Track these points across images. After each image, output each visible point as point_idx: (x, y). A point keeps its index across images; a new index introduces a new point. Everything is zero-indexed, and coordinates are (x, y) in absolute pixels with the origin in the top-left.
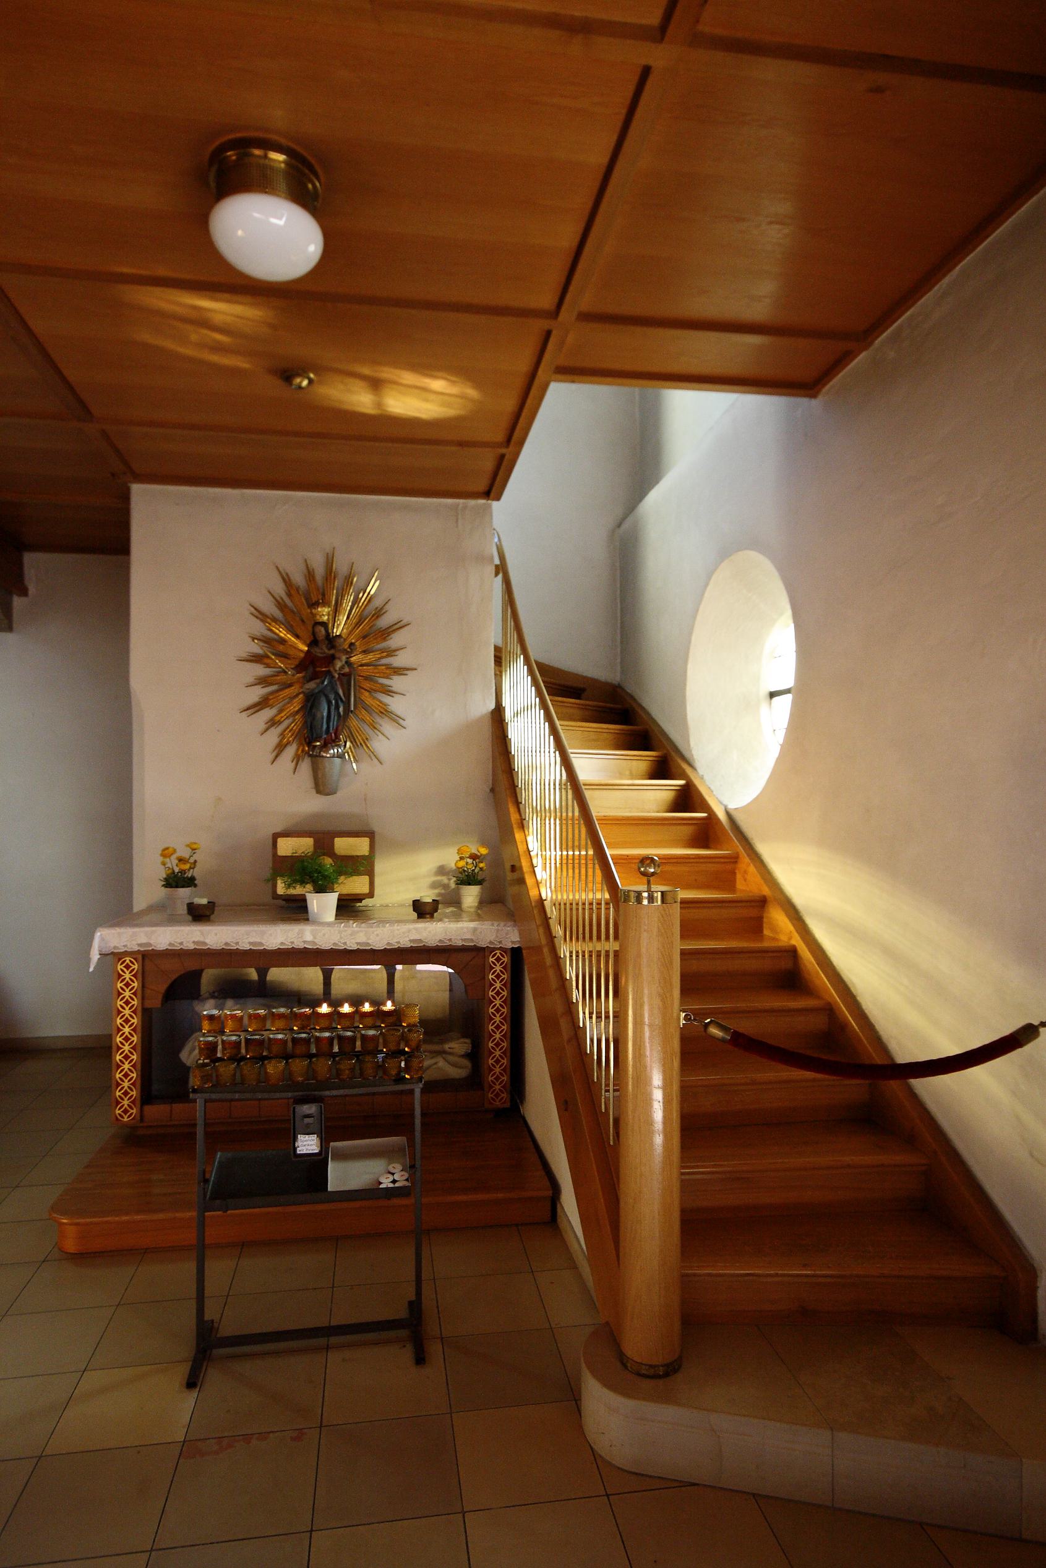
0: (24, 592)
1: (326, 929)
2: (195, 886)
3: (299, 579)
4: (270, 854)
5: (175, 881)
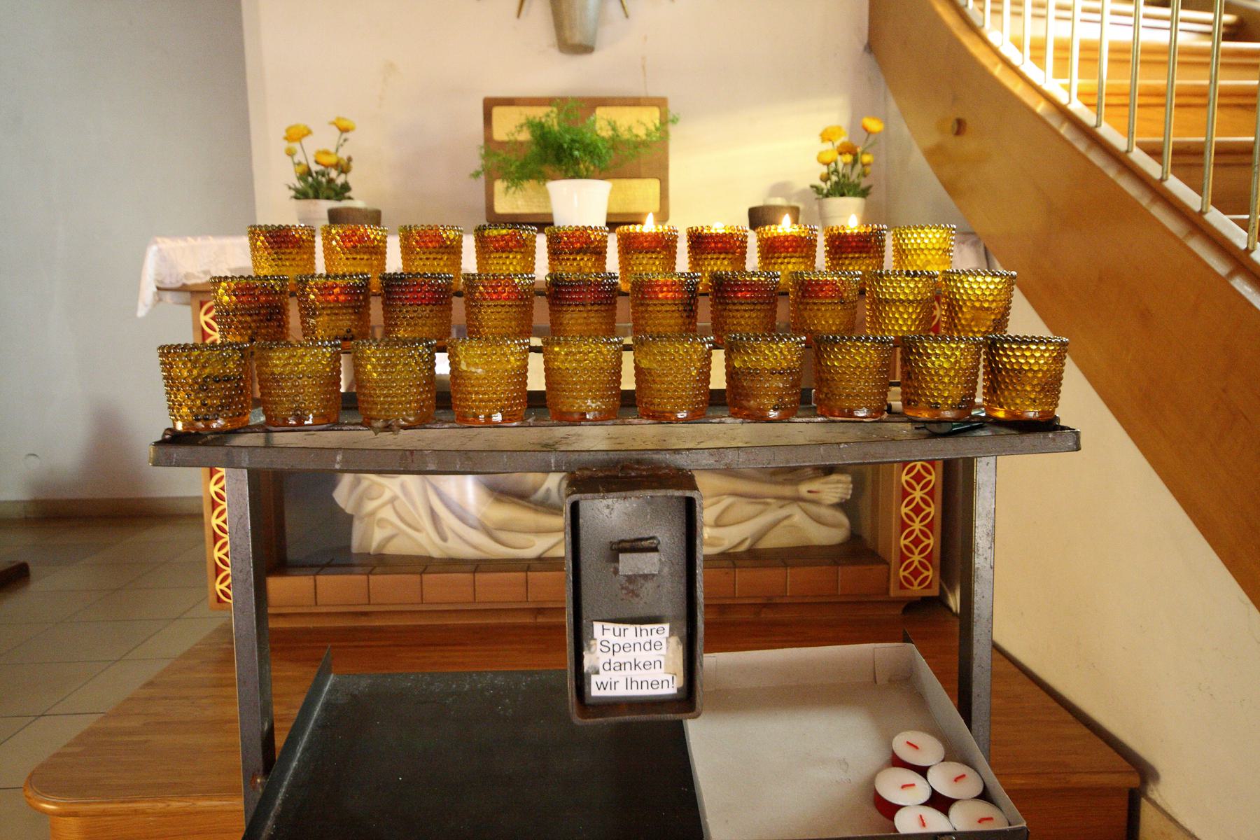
4: (481, 142)
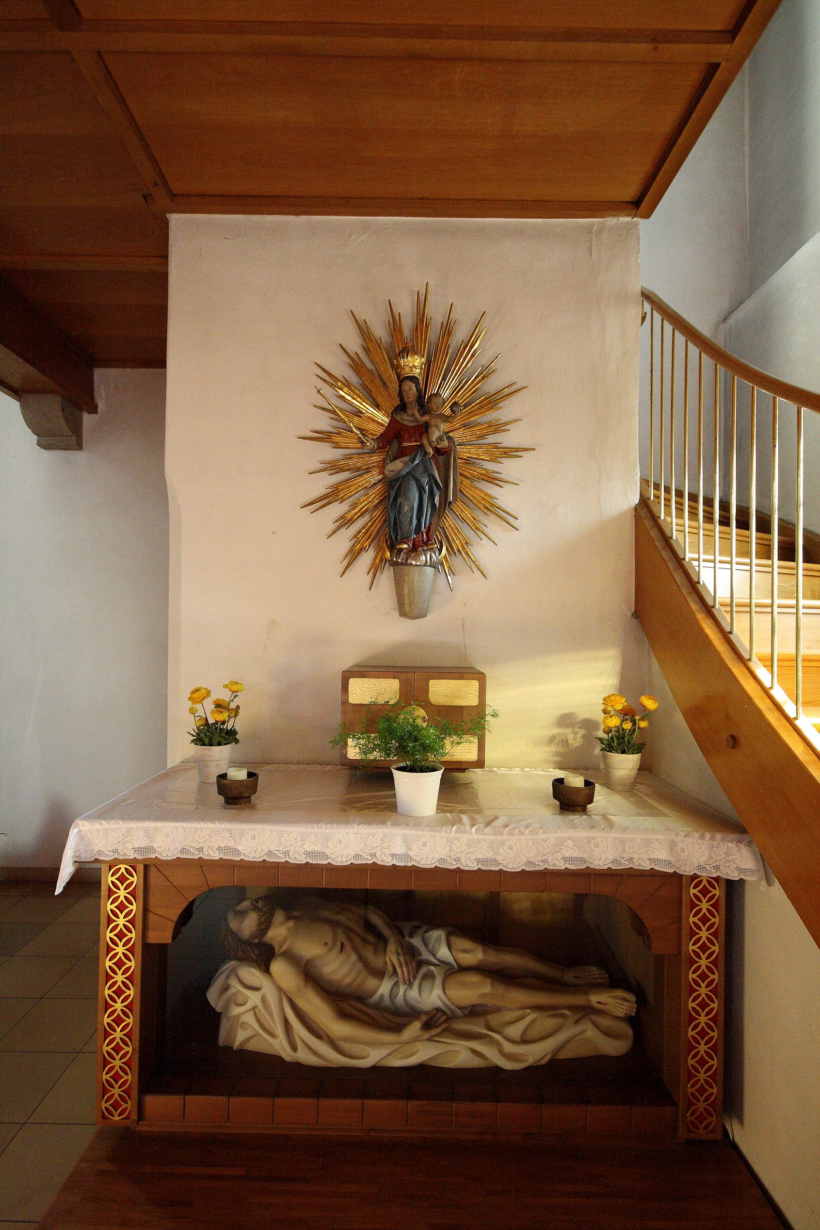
0: (94, 410)
1: (426, 835)
2: (237, 741)
3: (380, 331)
5: (211, 735)
